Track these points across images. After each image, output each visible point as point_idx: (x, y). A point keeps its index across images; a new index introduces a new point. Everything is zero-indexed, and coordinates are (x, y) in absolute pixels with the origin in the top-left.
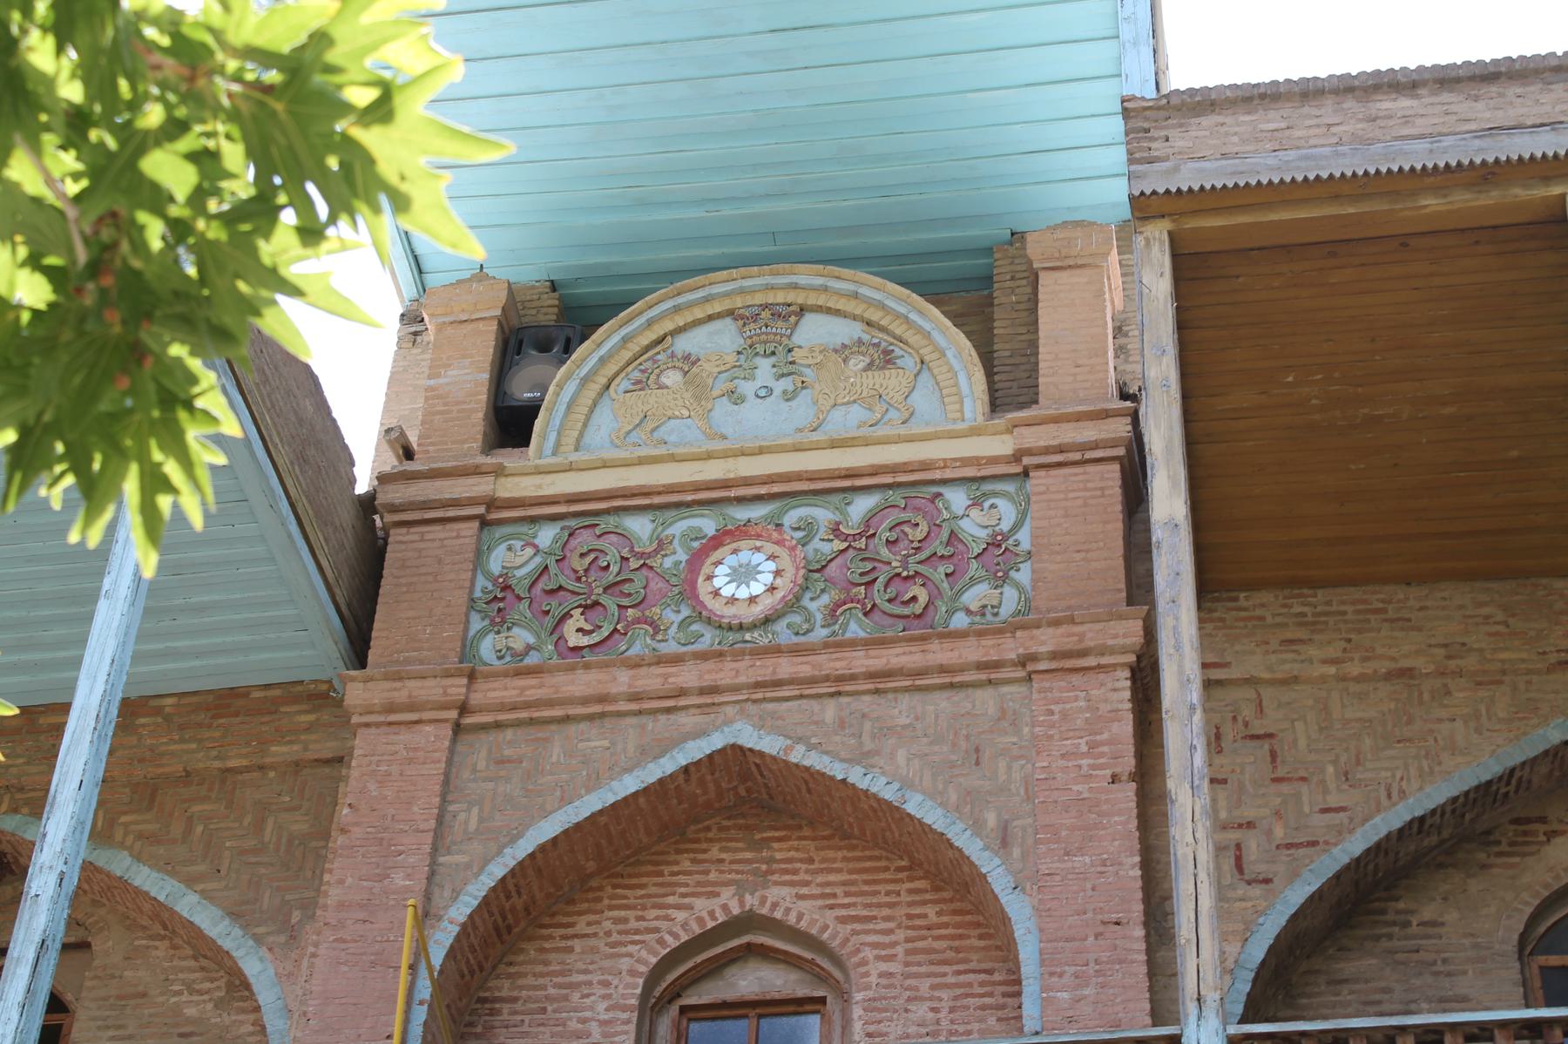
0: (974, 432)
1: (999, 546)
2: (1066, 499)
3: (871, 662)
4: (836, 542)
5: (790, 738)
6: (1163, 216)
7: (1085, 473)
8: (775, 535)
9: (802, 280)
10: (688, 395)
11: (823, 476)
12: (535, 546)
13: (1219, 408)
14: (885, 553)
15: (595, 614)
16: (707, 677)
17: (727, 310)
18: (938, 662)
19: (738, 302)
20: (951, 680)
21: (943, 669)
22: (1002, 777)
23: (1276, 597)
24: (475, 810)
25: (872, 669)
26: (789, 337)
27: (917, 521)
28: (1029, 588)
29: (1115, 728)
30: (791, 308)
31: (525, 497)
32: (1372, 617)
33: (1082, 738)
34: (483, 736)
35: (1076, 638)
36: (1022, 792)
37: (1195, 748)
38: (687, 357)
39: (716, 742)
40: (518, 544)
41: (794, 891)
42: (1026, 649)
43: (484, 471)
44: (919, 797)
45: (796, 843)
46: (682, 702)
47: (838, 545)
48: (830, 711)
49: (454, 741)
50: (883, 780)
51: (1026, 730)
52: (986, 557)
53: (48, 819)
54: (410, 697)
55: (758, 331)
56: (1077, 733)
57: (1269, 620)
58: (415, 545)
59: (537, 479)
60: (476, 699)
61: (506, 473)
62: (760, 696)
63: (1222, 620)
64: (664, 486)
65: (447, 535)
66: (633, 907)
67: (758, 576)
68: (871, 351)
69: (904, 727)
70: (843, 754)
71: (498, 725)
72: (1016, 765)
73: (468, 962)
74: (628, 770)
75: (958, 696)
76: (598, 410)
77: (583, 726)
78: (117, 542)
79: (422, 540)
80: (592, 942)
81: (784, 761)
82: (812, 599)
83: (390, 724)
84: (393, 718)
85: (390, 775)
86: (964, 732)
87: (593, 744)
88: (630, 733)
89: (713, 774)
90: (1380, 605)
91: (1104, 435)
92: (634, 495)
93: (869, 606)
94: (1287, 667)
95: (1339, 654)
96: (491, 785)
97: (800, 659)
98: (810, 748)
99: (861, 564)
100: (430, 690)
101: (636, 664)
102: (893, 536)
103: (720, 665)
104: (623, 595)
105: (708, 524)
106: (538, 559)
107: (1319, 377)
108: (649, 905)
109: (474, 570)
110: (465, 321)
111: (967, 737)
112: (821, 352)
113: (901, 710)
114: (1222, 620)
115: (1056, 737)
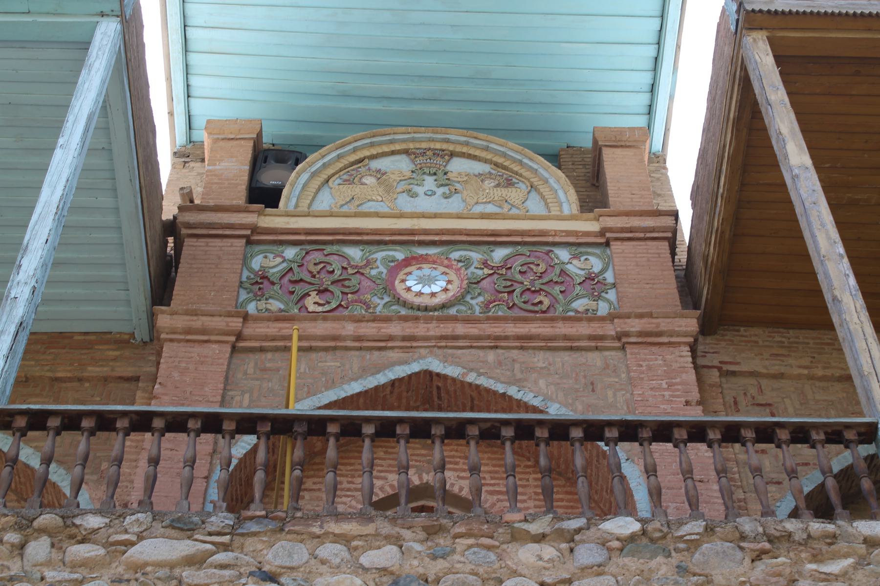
0: (572, 218)
1: (593, 280)
2: (636, 257)
3: (517, 330)
4: (485, 269)
5: (466, 369)
6: (761, 29)
7: (646, 245)
8: (446, 262)
9: (452, 137)
10: (381, 190)
11: (476, 233)
12: (283, 257)
13: (761, 182)
14: (519, 277)
15: (327, 296)
16: (407, 330)
17: (404, 149)
18: (563, 333)
19: (411, 146)
20: (571, 345)
21: (566, 338)
22: (611, 400)
23: (764, 332)
24: (247, 396)
25: (520, 334)
26: (445, 166)
27: (538, 262)
28: (615, 303)
29: (684, 376)
30: (445, 152)
31: (278, 228)
32: (826, 347)
33: (663, 380)
34: (251, 355)
35: (654, 325)
36: (625, 408)
37: (848, 275)
38: (379, 171)
39: (415, 367)
40: (271, 256)
41: (456, 474)
42: (622, 328)
43: (251, 210)
44: (557, 406)
45: (456, 447)
46: (390, 344)
47: (487, 271)
48: (491, 356)
49: (231, 357)
50: (532, 395)
51: (623, 376)
52: (585, 284)
53: (22, 257)
54: (203, 325)
55: (425, 161)
56: (659, 378)
57: (761, 343)
58: (202, 248)
59: (286, 219)
60: (248, 331)
61: (265, 213)
62: (443, 344)
63: (732, 341)
64: (371, 230)
65: (225, 244)
66: (347, 476)
67: (436, 282)
68: (498, 178)
69: (541, 368)
70: (502, 379)
71: (262, 350)
72: (619, 394)
73: (236, 490)
74: (355, 379)
75: (576, 355)
76: (320, 194)
77: (322, 354)
78: (67, 121)
79: (207, 246)
80: (317, 494)
81: (461, 381)
82: (472, 298)
83: (188, 341)
84: (189, 337)
85: (188, 369)
86: (582, 374)
87: (328, 364)
88: (354, 360)
89: (407, 392)
90: (830, 341)
91: (658, 224)
92: (351, 234)
93: (511, 304)
94: (777, 367)
95: (809, 364)
96: (258, 382)
97: (470, 325)
98: (480, 375)
99: (503, 282)
100: (218, 323)
101: (359, 320)
102: (524, 269)
103: (416, 325)
104: (343, 286)
105: (400, 255)
106: (285, 265)
107: (827, 165)
108: (356, 475)
109: (243, 267)
110: (232, 139)
111: (585, 377)
112: (466, 176)
113: (540, 359)
114: (732, 341)
115: (646, 379)
